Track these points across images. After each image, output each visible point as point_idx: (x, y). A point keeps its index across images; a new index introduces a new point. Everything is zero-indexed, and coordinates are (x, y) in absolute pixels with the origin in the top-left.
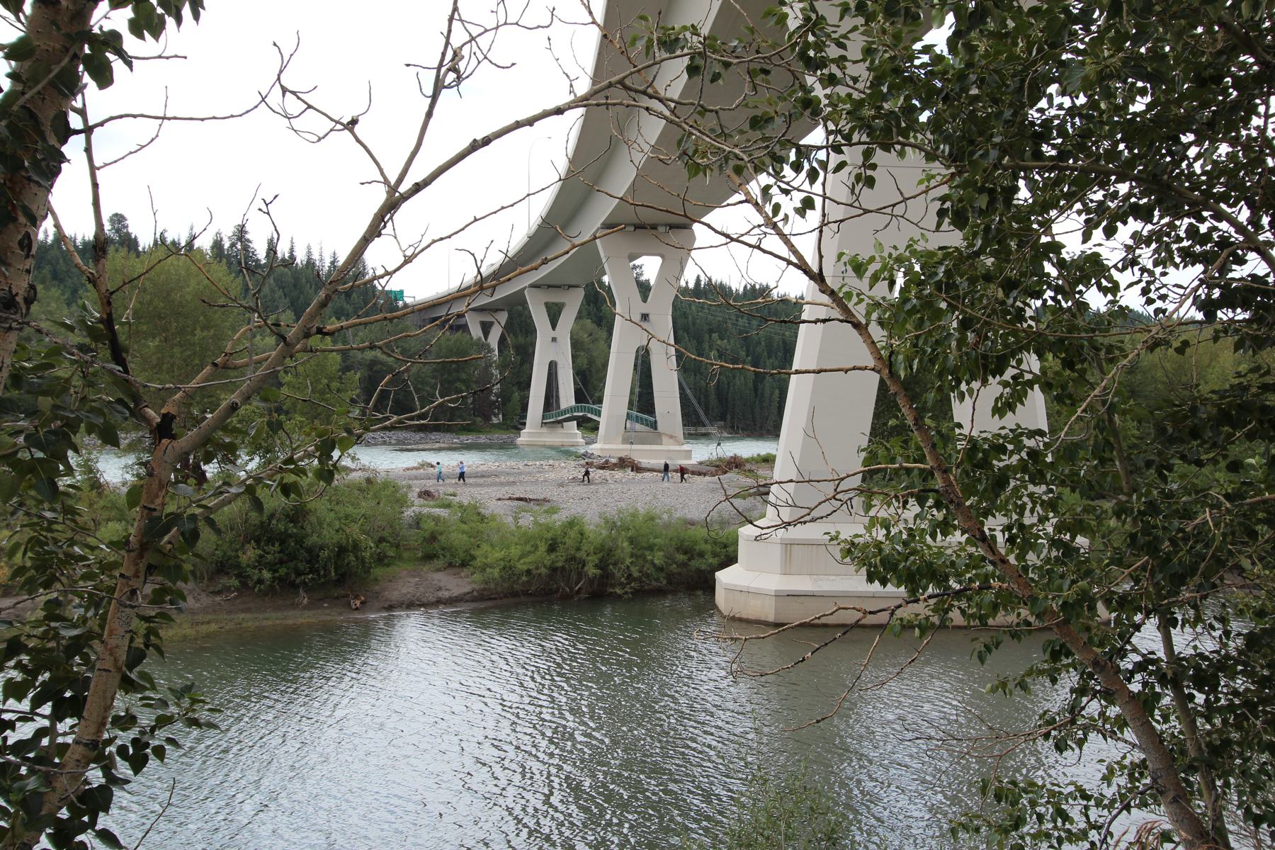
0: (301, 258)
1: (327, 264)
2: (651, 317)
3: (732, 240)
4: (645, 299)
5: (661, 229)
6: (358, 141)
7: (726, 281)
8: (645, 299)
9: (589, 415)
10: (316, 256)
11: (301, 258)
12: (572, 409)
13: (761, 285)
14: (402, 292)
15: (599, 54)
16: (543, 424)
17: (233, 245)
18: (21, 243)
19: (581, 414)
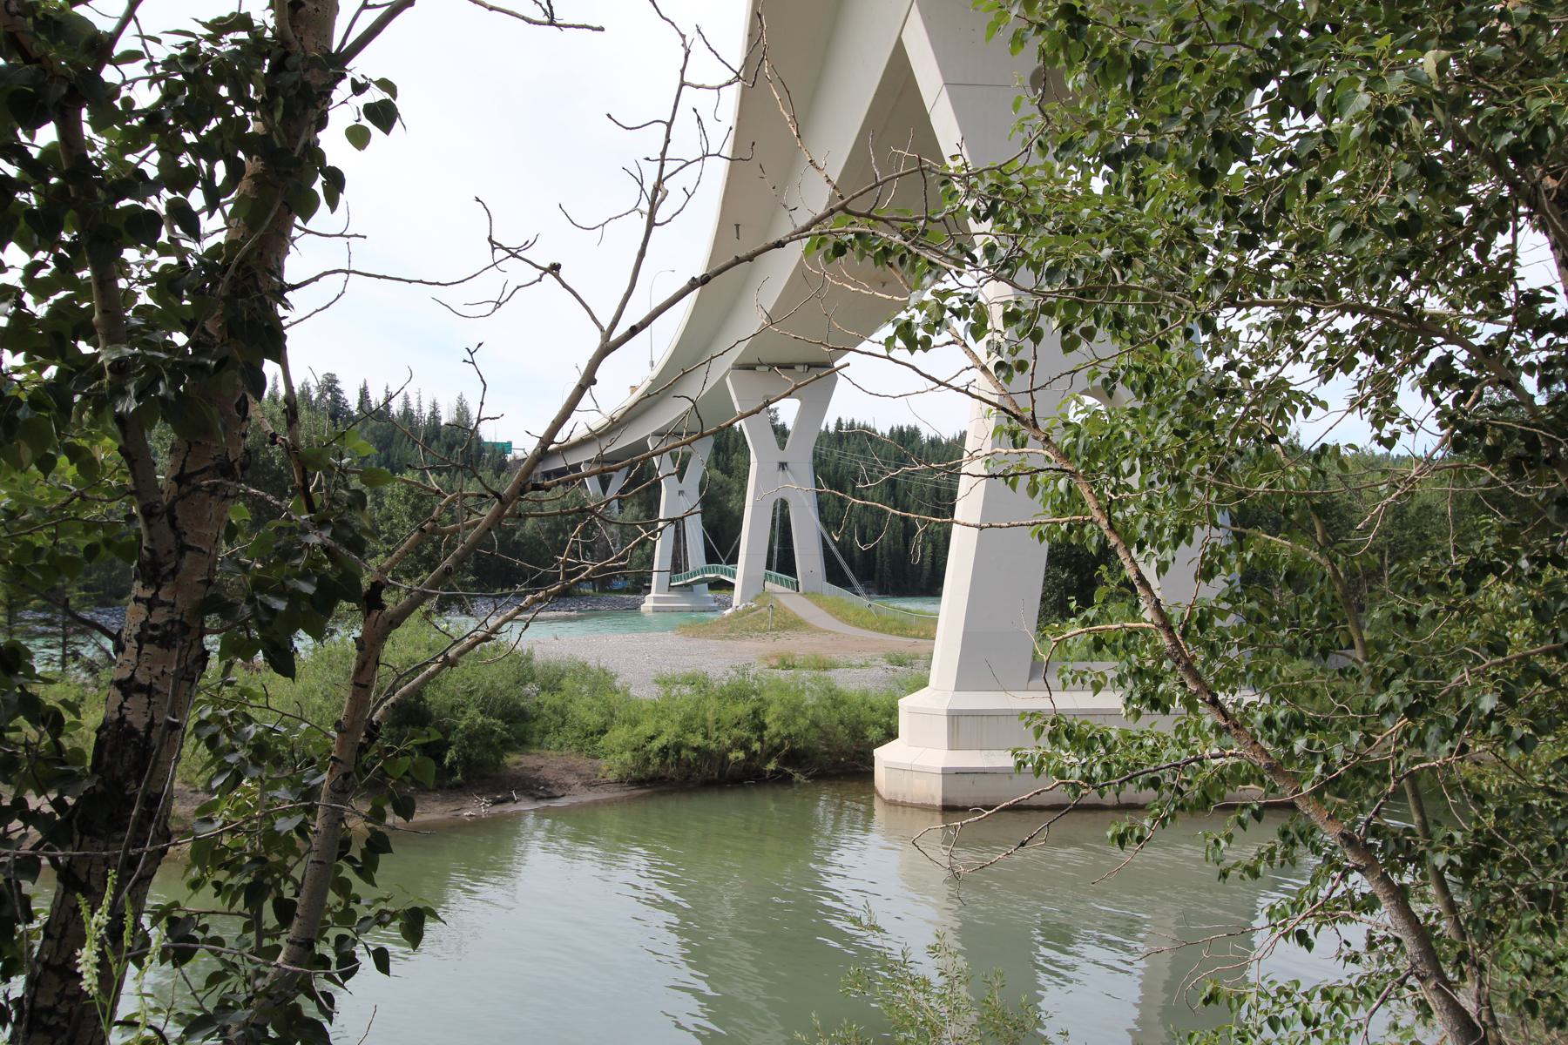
0: (396, 407)
1: (427, 411)
2: (789, 465)
3: (940, 384)
4: (782, 446)
5: (799, 369)
6: (565, 286)
7: (870, 423)
8: (782, 446)
9: (723, 577)
10: (414, 406)
11: (396, 407)
12: (703, 571)
13: (909, 427)
14: (510, 444)
15: (728, 178)
16: (671, 588)
17: (322, 396)
18: (238, 406)
19: (713, 575)
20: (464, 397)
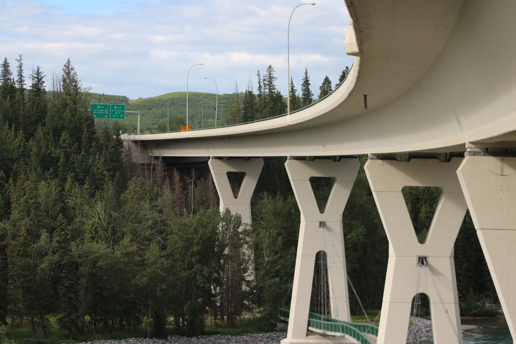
2: (430, 260)
20: (72, 64)
